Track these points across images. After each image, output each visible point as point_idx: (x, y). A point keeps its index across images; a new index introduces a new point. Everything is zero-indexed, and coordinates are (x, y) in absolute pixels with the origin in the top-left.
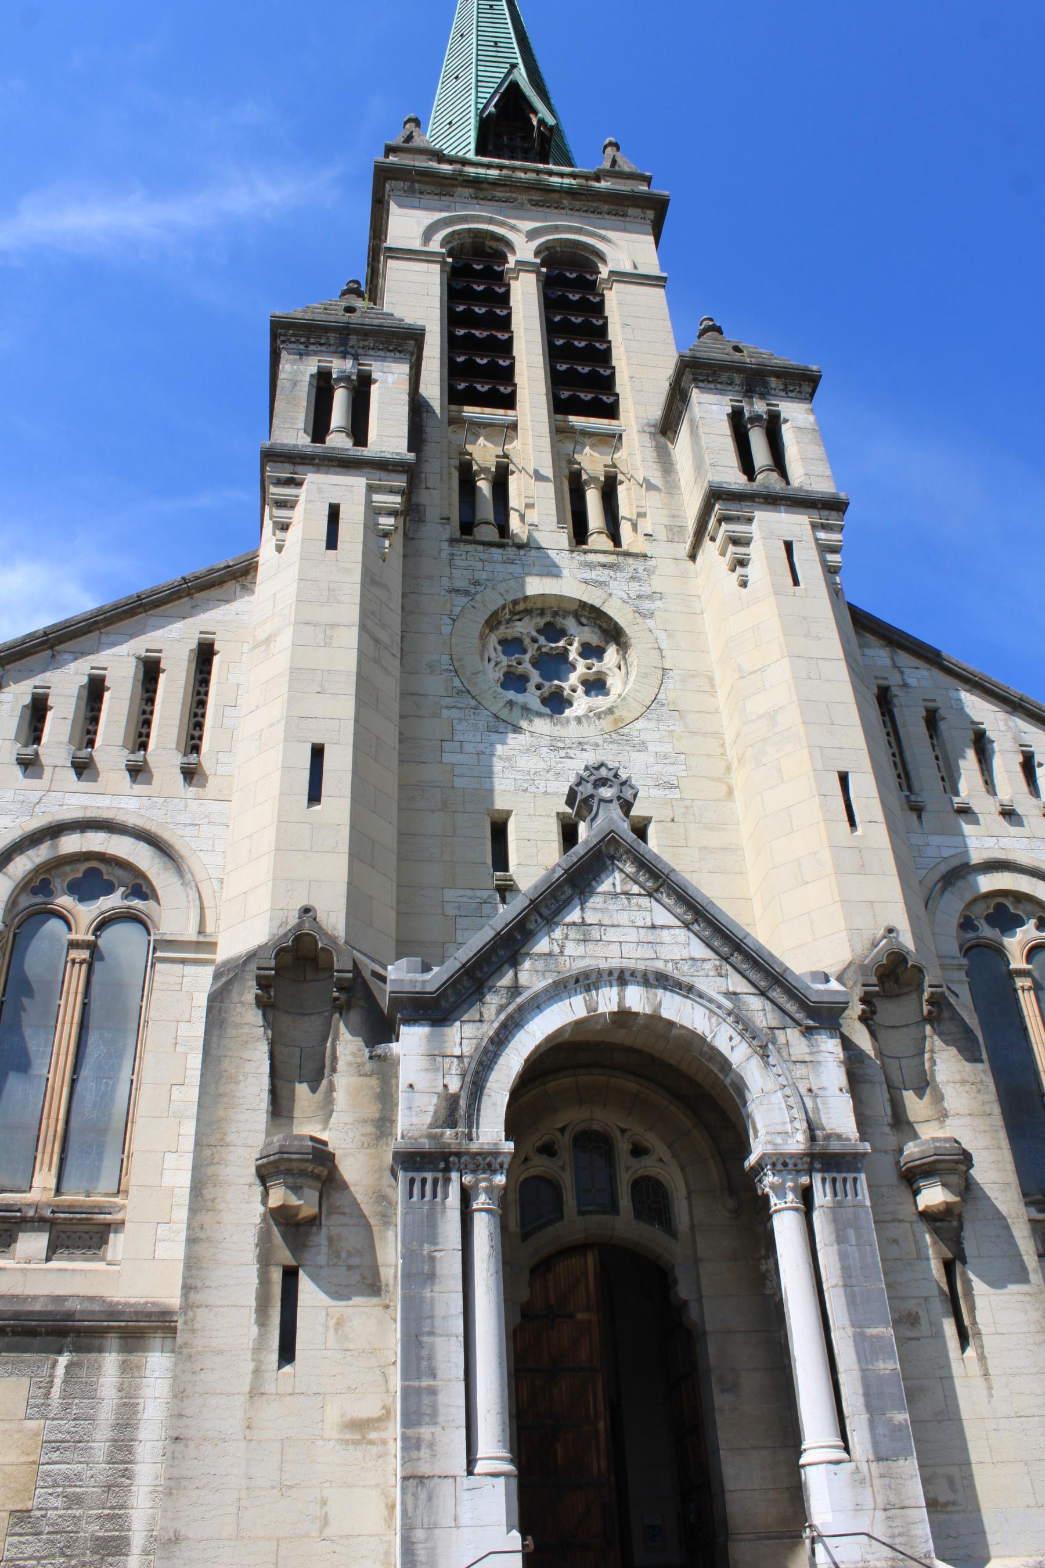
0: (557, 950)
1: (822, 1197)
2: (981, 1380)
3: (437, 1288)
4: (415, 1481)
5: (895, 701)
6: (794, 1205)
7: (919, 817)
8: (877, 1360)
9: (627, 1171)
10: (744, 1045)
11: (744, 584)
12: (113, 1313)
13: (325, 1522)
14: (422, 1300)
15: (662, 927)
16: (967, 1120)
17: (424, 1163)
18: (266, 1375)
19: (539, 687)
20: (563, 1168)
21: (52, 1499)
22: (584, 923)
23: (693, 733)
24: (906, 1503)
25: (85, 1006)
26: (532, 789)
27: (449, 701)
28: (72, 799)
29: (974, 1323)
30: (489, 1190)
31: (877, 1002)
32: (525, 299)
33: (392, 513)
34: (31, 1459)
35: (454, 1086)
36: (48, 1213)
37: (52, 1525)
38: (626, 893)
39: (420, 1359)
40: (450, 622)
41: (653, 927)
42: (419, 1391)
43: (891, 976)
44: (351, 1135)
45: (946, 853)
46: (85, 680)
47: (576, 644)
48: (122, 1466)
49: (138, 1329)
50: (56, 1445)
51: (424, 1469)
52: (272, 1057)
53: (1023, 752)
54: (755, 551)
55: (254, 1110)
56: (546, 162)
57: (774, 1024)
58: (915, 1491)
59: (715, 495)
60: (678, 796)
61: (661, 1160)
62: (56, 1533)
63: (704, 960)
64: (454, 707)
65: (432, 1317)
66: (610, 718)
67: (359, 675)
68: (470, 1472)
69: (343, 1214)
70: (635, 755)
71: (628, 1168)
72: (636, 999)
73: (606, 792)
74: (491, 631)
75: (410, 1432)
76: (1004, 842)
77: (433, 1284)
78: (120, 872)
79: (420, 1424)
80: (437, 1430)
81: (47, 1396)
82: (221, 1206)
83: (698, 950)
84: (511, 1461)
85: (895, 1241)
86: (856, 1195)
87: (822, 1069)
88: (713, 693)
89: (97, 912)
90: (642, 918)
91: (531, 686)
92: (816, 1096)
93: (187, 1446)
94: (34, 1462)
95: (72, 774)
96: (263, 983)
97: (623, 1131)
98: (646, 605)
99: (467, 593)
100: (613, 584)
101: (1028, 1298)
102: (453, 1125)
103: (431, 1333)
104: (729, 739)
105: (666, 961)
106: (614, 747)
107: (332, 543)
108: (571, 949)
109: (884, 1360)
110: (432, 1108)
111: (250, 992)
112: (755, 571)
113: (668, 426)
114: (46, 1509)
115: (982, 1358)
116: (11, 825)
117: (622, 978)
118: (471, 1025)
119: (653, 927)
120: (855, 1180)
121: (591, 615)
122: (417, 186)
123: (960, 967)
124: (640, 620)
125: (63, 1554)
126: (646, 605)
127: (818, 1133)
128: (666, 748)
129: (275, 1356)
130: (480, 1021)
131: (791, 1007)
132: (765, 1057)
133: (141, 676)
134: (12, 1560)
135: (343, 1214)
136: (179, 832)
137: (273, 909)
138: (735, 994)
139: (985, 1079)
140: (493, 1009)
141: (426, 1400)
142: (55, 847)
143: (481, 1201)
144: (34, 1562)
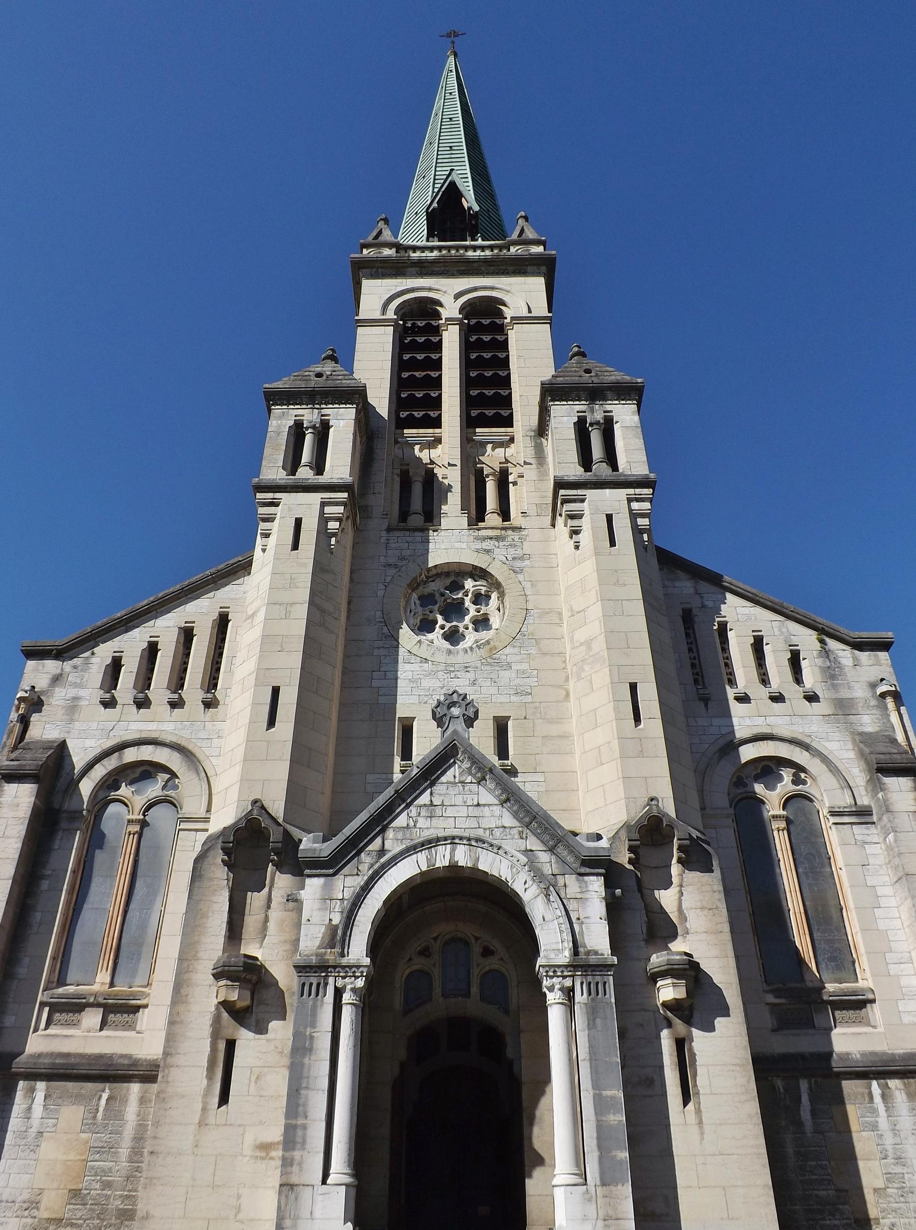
0: (412, 824)
1: (580, 998)
2: (697, 1127)
3: (313, 1057)
4: (287, 1188)
5: (696, 619)
6: (561, 1001)
7: (706, 705)
8: (609, 1114)
9: (479, 966)
10: (535, 887)
11: (577, 547)
12: (135, 1063)
13: (239, 1210)
14: (302, 1065)
15: (484, 805)
16: (704, 936)
17: (314, 971)
18: (210, 1112)
19: (442, 627)
20: (434, 965)
21: (94, 1183)
22: (432, 804)
23: (544, 654)
24: (620, 1216)
25: (136, 862)
27: (380, 643)
28: (134, 724)
29: (695, 1085)
30: (354, 990)
31: (641, 851)
32: (451, 342)
33: (339, 520)
34: (83, 1158)
35: (337, 919)
36: (101, 1000)
37: (94, 1199)
39: (298, 1105)
40: (383, 587)
41: (478, 805)
42: (295, 1127)
43: (650, 833)
44: (276, 951)
46: (145, 645)
48: (136, 1165)
49: (147, 1073)
50: (99, 1150)
51: (294, 1179)
52: (231, 900)
53: (791, 651)
54: (585, 523)
55: (217, 936)
57: (556, 872)
58: (628, 1207)
59: (560, 484)
60: (530, 700)
61: (502, 959)
62: (95, 1204)
63: (511, 828)
64: (383, 647)
65: (308, 1077)
66: (487, 647)
67: (307, 637)
68: (324, 1182)
69: (267, 1004)
70: (502, 673)
71: (478, 965)
72: (462, 856)
73: (455, 711)
74: (413, 591)
75: (287, 1154)
76: (770, 720)
77: (310, 1055)
79: (294, 1149)
80: (305, 1153)
81: (95, 1117)
82: (191, 1000)
83: (508, 820)
84: (352, 1176)
85: (641, 1025)
86: (605, 994)
87: (588, 903)
88: (560, 625)
89: (146, 800)
90: (472, 800)
92: (582, 923)
93: (158, 1157)
94: (84, 1160)
95: (134, 708)
96: (226, 851)
97: (477, 939)
98: (518, 564)
99: (396, 566)
100: (497, 551)
101: (738, 1068)
102: (332, 947)
103: (307, 1088)
104: (568, 655)
105: (485, 829)
106: (488, 668)
107: (295, 546)
108: (422, 823)
109: (614, 1114)
110: (321, 935)
111: (218, 856)
112: (585, 538)
113: (542, 430)
114: (91, 1190)
115: (698, 1111)
116: (95, 745)
117: (452, 840)
118: (350, 878)
120: (605, 983)
121: (479, 573)
123: (728, 816)
124: (513, 575)
125: (99, 1218)
126: (518, 564)
127: (581, 950)
128: (525, 666)
129: (216, 1100)
130: (357, 875)
131: (570, 859)
132: (547, 896)
133: (182, 641)
134: (69, 1219)
135: (267, 1004)
136: (199, 744)
137: (239, 800)
138: (532, 851)
139: (720, 905)
140: (366, 866)
141: (299, 1133)
142: (120, 758)
143: (347, 997)
144: (82, 1222)
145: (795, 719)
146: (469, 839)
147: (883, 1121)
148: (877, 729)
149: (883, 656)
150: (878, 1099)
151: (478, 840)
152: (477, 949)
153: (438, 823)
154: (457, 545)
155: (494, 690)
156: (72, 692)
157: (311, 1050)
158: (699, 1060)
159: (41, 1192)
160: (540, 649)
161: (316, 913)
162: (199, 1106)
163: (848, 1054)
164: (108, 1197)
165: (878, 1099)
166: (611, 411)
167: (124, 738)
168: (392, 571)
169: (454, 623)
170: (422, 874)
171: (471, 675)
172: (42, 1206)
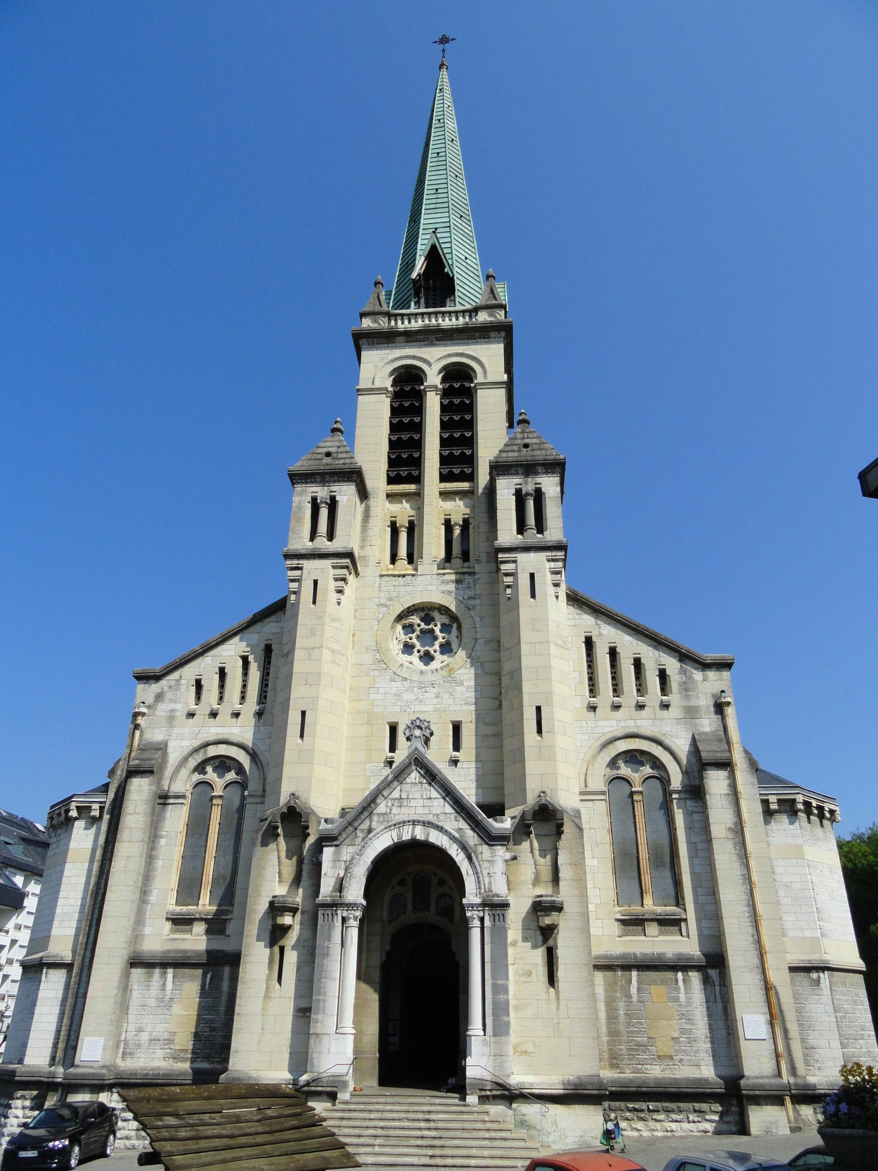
1: (487, 923)
26: (408, 710)
27: (374, 667)
28: (214, 730)
32: (433, 404)
38: (421, 783)
41: (430, 798)
45: (606, 730)
47: (439, 626)
56: (445, 306)
66: (448, 669)
72: (420, 833)
78: (233, 762)
83: (449, 809)
91: (415, 650)
97: (435, 874)
103: (326, 978)
106: (448, 684)
108: (395, 810)
119: (430, 798)
122: (375, 340)
140: (360, 839)
141: (321, 1004)
142: (205, 753)
145: (657, 722)
146: (424, 822)
147: (682, 997)
148: (713, 729)
149: (726, 674)
150: (681, 983)
151: (429, 823)
152: (435, 881)
153: (404, 810)
154: (429, 587)
155: (451, 701)
156: (172, 706)
157: (327, 954)
158: (560, 961)
159: (174, 1034)
160: (483, 670)
161: (330, 870)
162: (265, 986)
163: (664, 954)
164: (214, 1036)
165: (681, 983)
166: (540, 484)
167: (207, 739)
168: (383, 609)
169: (427, 648)
170: (395, 844)
171: (435, 691)
172: (176, 1042)
